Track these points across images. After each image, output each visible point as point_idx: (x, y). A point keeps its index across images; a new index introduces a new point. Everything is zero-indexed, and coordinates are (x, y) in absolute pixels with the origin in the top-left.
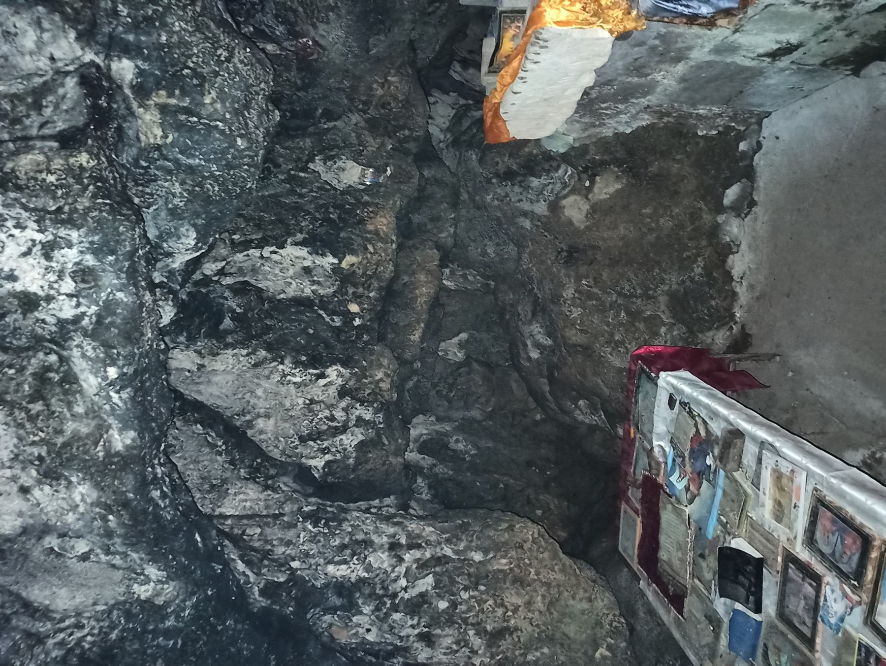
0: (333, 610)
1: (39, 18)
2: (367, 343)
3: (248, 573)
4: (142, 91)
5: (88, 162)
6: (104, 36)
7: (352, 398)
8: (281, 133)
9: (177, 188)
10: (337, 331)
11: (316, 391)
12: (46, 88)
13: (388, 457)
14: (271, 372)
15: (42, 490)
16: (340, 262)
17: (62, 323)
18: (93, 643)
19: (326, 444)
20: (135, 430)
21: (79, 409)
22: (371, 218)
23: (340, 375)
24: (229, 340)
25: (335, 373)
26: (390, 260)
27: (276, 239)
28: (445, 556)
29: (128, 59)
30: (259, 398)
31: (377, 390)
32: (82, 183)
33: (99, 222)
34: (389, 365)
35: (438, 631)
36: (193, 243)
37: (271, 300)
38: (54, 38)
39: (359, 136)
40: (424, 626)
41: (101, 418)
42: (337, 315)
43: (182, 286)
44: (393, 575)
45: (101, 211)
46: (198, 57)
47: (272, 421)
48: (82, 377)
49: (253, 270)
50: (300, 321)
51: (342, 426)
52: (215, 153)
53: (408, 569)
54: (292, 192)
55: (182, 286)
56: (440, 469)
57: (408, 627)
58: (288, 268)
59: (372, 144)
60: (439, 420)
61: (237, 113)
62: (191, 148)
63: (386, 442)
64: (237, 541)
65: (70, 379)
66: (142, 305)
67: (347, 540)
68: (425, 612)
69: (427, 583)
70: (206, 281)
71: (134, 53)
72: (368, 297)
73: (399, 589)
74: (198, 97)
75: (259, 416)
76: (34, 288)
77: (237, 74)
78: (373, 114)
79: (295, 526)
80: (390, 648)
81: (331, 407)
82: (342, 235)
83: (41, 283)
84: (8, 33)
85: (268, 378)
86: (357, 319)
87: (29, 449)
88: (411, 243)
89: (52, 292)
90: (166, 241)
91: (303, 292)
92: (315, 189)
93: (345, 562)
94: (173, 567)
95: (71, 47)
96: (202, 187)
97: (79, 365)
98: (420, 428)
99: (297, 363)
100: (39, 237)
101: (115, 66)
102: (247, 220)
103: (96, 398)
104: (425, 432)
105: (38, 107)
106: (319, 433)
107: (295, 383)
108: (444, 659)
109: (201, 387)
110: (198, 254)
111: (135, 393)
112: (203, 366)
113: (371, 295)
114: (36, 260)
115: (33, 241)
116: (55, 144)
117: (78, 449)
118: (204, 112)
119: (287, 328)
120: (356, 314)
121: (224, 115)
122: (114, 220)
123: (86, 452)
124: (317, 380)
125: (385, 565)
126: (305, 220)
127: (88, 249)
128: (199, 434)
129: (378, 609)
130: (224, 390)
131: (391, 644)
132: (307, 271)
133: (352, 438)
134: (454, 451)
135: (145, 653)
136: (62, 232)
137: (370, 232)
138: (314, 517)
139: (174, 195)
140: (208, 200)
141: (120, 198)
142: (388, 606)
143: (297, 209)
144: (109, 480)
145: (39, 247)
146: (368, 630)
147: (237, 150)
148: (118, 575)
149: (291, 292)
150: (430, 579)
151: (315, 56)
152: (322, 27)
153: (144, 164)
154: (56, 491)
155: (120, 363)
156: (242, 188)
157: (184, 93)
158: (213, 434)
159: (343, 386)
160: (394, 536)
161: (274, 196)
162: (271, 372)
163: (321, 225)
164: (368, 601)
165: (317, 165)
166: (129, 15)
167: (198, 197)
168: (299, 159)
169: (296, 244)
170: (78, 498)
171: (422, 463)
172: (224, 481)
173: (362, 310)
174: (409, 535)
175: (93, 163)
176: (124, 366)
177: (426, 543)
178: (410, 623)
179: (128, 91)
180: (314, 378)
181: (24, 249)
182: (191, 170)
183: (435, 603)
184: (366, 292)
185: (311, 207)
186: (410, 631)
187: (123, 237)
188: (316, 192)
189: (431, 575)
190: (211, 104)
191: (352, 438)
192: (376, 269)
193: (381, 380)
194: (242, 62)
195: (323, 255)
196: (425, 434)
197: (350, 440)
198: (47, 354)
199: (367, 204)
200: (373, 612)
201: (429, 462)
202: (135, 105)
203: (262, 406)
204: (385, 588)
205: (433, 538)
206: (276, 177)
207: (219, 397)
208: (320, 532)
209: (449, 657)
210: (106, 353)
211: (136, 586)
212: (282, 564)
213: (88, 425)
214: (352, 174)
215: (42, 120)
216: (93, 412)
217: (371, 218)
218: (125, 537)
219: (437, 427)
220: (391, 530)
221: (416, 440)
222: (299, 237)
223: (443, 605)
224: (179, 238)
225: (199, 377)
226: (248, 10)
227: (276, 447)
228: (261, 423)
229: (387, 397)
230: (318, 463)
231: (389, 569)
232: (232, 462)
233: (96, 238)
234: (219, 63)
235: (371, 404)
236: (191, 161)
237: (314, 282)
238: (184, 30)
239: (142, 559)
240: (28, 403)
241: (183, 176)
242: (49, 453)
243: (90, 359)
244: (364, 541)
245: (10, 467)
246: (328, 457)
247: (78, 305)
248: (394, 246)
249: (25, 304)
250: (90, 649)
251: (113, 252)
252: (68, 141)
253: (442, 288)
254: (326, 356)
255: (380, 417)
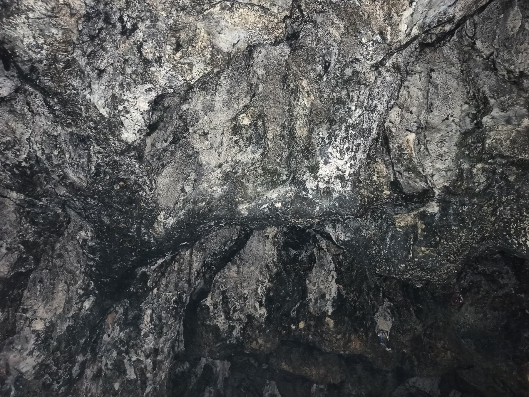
0: (125, 314)
1: (452, 170)
2: (280, 332)
3: (156, 265)
4: (423, 216)
5: (385, 194)
6: (450, 199)
7: (247, 323)
8: (405, 286)
9: (371, 232)
10: (287, 314)
11: (251, 301)
12: (418, 174)
13: (209, 346)
14: (264, 275)
15: (220, 173)
16: (329, 317)
17: (303, 183)
18: (142, 195)
19: (220, 307)
20: (248, 215)
21: (259, 189)
22: (359, 337)
23: (261, 316)
24: (283, 253)
25: (263, 313)
26: (333, 350)
27: (342, 279)
28: (146, 387)
29: (439, 210)
30: (249, 268)
31: (251, 340)
32: (374, 191)
33: (356, 199)
34: (267, 347)
35: (101, 382)
36: (342, 239)
37: (306, 276)
38: (443, 176)
39: (409, 330)
40: (105, 373)
41: (255, 199)
42: (297, 314)
43: (315, 230)
44: (139, 351)
45: (361, 200)
46: (447, 245)
47: (235, 275)
48: (276, 191)
49: (322, 265)
50: (293, 292)
51: (230, 317)
52: (394, 253)
53: (141, 362)
54: (370, 288)
55: (315, 230)
56: (194, 380)
57: (107, 362)
58: (324, 285)
59: (405, 339)
60: (226, 380)
61: (419, 265)
62: (396, 240)
63: (218, 345)
64: (173, 259)
65: (274, 185)
66: (313, 218)
67: (164, 321)
68: (114, 373)
69: (131, 374)
70: (316, 241)
71: (443, 212)
72: (309, 334)
73: (130, 355)
74: (424, 244)
75: (239, 267)
76: (320, 171)
77: (441, 264)
78: (425, 341)
79: (176, 290)
80: (97, 350)
81: (242, 310)
82: (346, 318)
83: (324, 174)
84: (442, 157)
85: (261, 273)
86: (294, 327)
87: (240, 168)
88: (343, 363)
89: (319, 179)
90: (342, 225)
91: (310, 293)
92: (373, 302)
93: (152, 320)
94: (173, 232)
95: (440, 184)
96: (373, 245)
97: (282, 190)
98: (221, 367)
99: (269, 290)
100: (347, 174)
101: (434, 203)
102: (351, 263)
103: (265, 197)
104: (218, 369)
105: (408, 170)
106: (227, 303)
107: (257, 289)
108: (84, 387)
109: (257, 238)
110: (334, 240)
111: (267, 215)
112: (268, 238)
113: (310, 336)
114: (335, 173)
115: (345, 172)
116: (392, 179)
117: (240, 189)
118: (416, 247)
119: (289, 284)
120: (297, 326)
121: (417, 258)
122: (357, 206)
123: (238, 193)
124: (259, 302)
125: (146, 346)
126: (354, 296)
127: (342, 194)
128: (232, 237)
129: (121, 341)
130: (254, 249)
131: (100, 351)
132: (323, 296)
133: (222, 322)
134: (204, 390)
135: (130, 218)
136: (349, 183)
137: (350, 337)
138: (179, 301)
139: (367, 230)
140: (367, 247)
141: (369, 208)
142: (122, 349)
143: (360, 292)
144: (224, 203)
145: (341, 174)
146: (109, 336)
147: (398, 264)
148: (171, 205)
149: (310, 286)
150: (133, 376)
151: (453, 304)
152: (472, 309)
153: (384, 216)
154: (219, 179)
155: (283, 209)
156: (376, 266)
157: (425, 237)
158: (231, 245)
159: (254, 317)
160: (162, 351)
161: (366, 278)
162: (264, 275)
163: (351, 306)
164: (127, 336)
165: (387, 303)
166: (463, 211)
167: (367, 242)
168: (390, 293)
169: (339, 290)
170: (215, 189)
171: (199, 367)
172: (204, 250)
173: (301, 330)
174: (162, 362)
175: (385, 196)
176: (282, 210)
177: (155, 374)
178: (109, 363)
179: (422, 209)
180: (260, 300)
181: (340, 168)
182: (383, 240)
183: (119, 380)
184: (312, 333)
185: (361, 300)
186: (104, 363)
187: (348, 210)
188: (371, 303)
189: (135, 377)
190: (421, 251)
191: (222, 322)
192: (327, 340)
193: (257, 342)
194: (448, 267)
195: (333, 306)
196: (216, 370)
197: (221, 322)
198: (286, 175)
199: (367, 335)
200: (120, 339)
201: (198, 372)
202: (415, 213)
203: (245, 270)
204: (132, 347)
205: (158, 379)
206: (378, 279)
207: (250, 246)
208: (170, 304)
209: (84, 391)
210: (289, 202)
211: (164, 213)
212: (157, 284)
213: (251, 193)
214: (384, 324)
215: (402, 171)
216: (258, 196)
217: (359, 337)
218: (193, 210)
219: (220, 378)
220: (166, 350)
221: (213, 363)
222: (344, 293)
223: (117, 386)
224: (344, 232)
225: (262, 237)
226: (472, 265)
227: (220, 277)
228: (234, 269)
229: (246, 346)
230: (208, 302)
231: (143, 349)
232: (215, 254)
233: (347, 198)
234: (446, 256)
235: (243, 335)
236: (388, 240)
237: (316, 300)
238: (461, 238)
239: (179, 217)
240: (262, 166)
241: (379, 235)
242: (239, 176)
243: (285, 195)
244: (162, 332)
245: (232, 160)
246: (211, 308)
247: (313, 190)
248: (342, 352)
249: (313, 167)
250: (139, 194)
251: (340, 205)
252: (395, 185)
253: (312, 383)
254: (272, 308)
255: (234, 341)
